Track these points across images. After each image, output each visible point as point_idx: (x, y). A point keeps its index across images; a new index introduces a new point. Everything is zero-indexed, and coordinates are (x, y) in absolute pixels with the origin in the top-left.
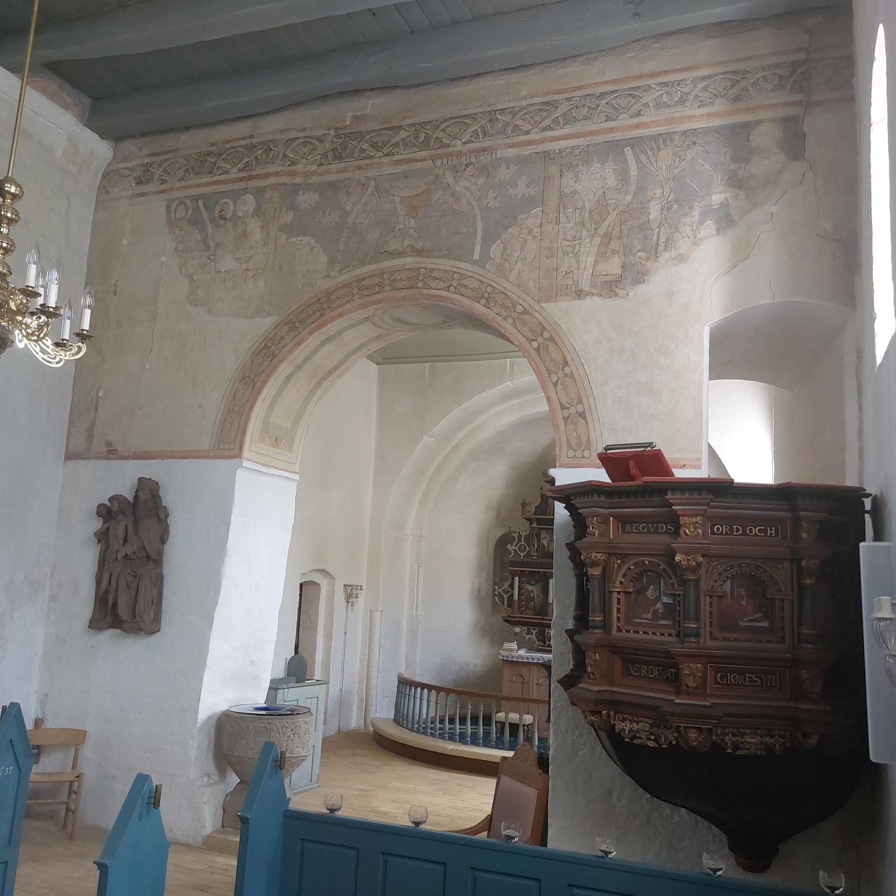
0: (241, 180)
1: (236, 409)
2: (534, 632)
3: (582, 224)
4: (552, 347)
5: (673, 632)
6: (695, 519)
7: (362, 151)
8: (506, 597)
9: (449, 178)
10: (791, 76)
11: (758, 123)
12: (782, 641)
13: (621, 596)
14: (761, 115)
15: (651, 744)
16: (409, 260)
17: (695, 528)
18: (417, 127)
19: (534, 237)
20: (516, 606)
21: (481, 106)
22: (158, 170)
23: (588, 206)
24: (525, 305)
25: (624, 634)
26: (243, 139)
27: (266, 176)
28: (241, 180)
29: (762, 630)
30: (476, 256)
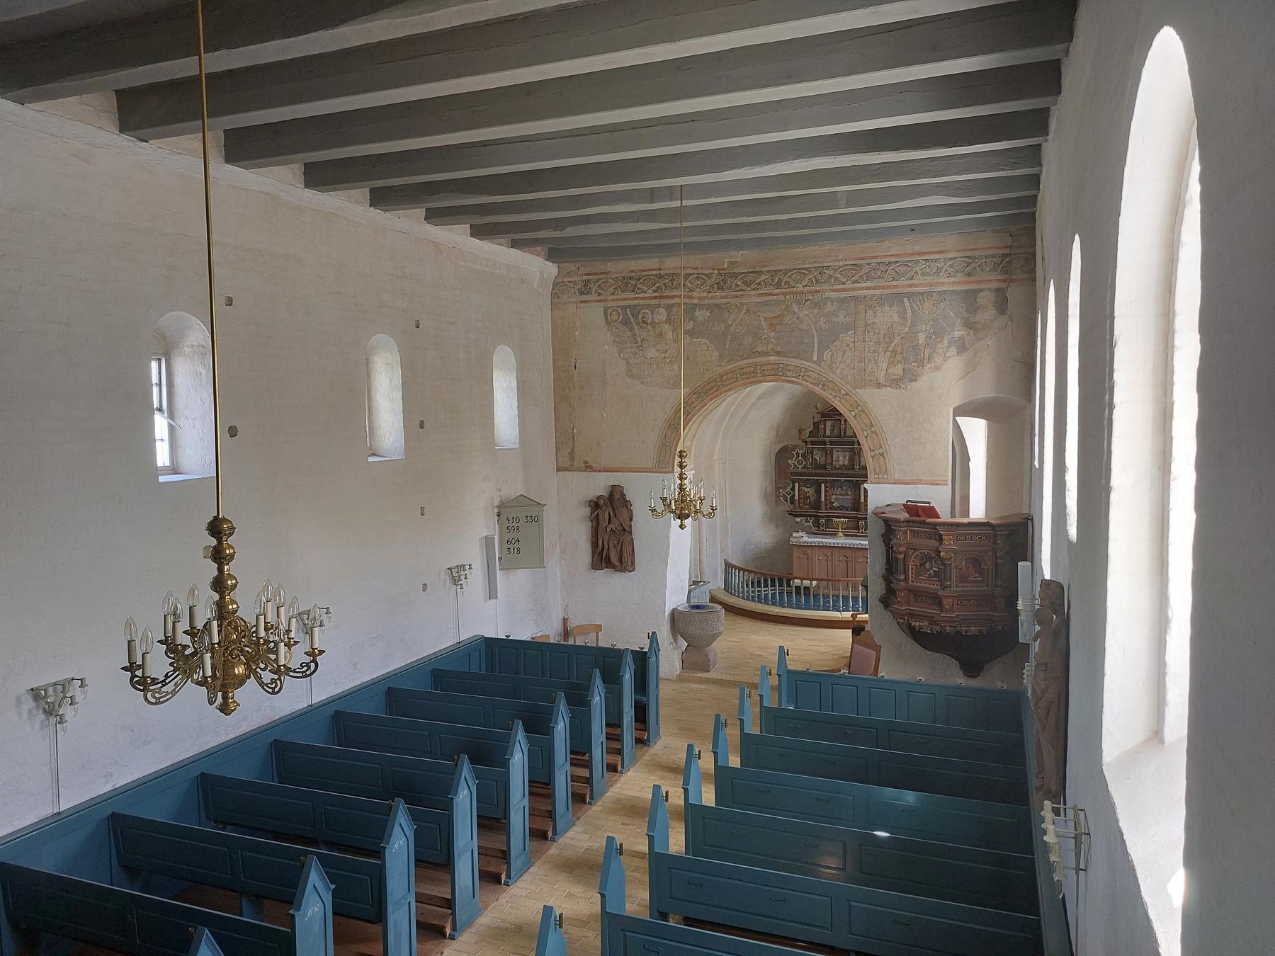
0: (655, 298)
1: (668, 444)
2: (811, 521)
3: (879, 343)
4: (863, 415)
5: (939, 584)
6: (949, 537)
7: (737, 285)
8: (788, 497)
9: (795, 307)
10: (1001, 263)
11: (982, 290)
12: (988, 586)
13: (914, 567)
14: (984, 286)
15: (929, 631)
16: (772, 358)
17: (950, 541)
18: (773, 273)
19: (850, 349)
20: (797, 503)
21: (814, 263)
22: (594, 285)
23: (882, 333)
24: (846, 390)
25: (915, 584)
26: (654, 270)
27: (673, 297)
28: (655, 298)
29: (980, 581)
30: (815, 359)
